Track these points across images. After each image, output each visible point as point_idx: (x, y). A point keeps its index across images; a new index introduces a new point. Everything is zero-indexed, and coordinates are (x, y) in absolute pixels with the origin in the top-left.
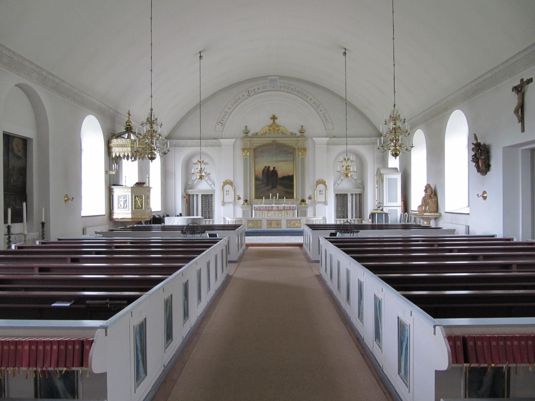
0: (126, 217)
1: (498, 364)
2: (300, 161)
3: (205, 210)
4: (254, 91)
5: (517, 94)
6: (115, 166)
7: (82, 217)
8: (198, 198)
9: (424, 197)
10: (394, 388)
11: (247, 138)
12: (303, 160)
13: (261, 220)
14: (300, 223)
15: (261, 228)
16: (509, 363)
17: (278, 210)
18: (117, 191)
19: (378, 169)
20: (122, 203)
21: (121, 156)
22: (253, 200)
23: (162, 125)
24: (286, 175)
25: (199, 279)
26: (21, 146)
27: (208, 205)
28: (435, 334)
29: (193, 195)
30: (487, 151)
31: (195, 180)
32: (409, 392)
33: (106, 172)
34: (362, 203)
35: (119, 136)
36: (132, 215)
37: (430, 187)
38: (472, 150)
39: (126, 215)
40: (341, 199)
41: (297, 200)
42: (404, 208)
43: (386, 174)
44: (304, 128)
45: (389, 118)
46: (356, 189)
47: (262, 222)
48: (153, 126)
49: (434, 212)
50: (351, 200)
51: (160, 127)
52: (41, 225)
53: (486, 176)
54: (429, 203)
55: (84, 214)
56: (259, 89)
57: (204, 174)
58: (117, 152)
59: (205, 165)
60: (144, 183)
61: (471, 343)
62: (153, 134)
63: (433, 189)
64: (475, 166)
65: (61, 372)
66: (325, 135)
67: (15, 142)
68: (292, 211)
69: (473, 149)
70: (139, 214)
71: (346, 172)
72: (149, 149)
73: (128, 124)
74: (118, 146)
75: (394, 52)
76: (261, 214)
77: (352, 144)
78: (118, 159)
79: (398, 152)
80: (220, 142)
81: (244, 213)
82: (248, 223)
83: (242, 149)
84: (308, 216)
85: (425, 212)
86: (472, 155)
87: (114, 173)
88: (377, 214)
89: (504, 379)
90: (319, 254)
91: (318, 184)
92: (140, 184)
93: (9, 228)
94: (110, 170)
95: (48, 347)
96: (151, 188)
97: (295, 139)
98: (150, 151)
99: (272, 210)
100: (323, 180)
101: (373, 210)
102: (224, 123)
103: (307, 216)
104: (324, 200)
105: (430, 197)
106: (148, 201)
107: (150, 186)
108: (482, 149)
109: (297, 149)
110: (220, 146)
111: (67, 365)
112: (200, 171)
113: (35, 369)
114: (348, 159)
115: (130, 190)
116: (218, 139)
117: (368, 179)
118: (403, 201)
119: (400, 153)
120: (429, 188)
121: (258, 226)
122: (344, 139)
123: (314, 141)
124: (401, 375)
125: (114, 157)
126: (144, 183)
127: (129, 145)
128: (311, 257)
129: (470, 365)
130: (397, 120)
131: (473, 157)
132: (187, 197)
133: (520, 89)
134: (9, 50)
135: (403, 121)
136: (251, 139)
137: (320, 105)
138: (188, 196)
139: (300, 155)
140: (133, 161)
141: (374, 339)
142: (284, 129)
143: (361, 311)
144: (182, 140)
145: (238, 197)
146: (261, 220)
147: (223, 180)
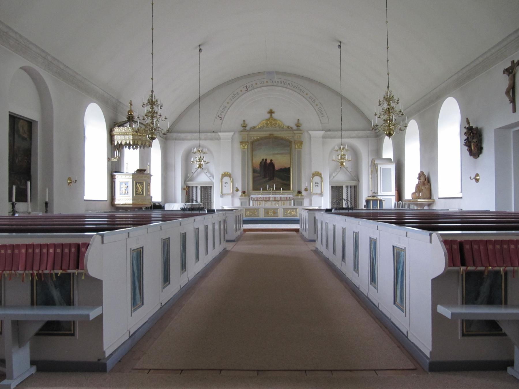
0: (127, 203)
1: (495, 267)
2: (296, 154)
3: (204, 202)
4: (252, 87)
5: (508, 75)
6: (116, 153)
7: (85, 200)
8: (197, 190)
9: (417, 185)
10: (390, 320)
11: (245, 131)
12: (299, 153)
13: (259, 209)
14: (296, 212)
15: (259, 217)
16: (506, 267)
17: (275, 200)
18: (119, 178)
19: (373, 159)
20: (123, 189)
21: (123, 144)
22: (251, 192)
23: (162, 106)
24: (283, 167)
25: (197, 242)
26: (26, 128)
27: (207, 197)
28: (431, 242)
29: (193, 187)
30: (479, 134)
31: (194, 173)
32: (406, 316)
33: (109, 159)
34: (357, 195)
35: (121, 125)
36: (133, 201)
37: (423, 175)
38: (465, 134)
39: (127, 201)
40: (337, 191)
41: (294, 192)
42: (398, 198)
43: (380, 164)
44: (301, 122)
45: (383, 99)
46: (353, 182)
47: (259, 211)
48: (154, 107)
49: (428, 199)
50: (346, 192)
51: (161, 108)
52: (44, 205)
53: (479, 159)
54: (422, 190)
55: (86, 198)
56: (256, 84)
57: (203, 163)
58: (119, 140)
59: (204, 154)
60: (145, 170)
61: (467, 247)
62: (153, 115)
63: (427, 176)
64: (467, 150)
65: (57, 274)
66: (321, 129)
67: (21, 123)
68: (289, 201)
69: (465, 133)
70: (140, 200)
71: (341, 161)
72: (149, 129)
73: (130, 114)
74: (120, 134)
75: (387, 35)
76: (258, 204)
77: (346, 138)
78: (119, 147)
79: (392, 132)
80: (219, 135)
81: (242, 203)
82: (246, 211)
83: (240, 142)
84: (304, 205)
85: (419, 199)
86: (465, 139)
87: (116, 160)
88: (371, 201)
89: (502, 289)
90: (315, 234)
91: (314, 176)
92: (141, 171)
93: (13, 205)
94: (112, 157)
95: (45, 251)
96: (151, 175)
97: (291, 132)
98: (151, 132)
99: (269, 200)
100: (319, 172)
101: (368, 196)
102: (222, 117)
103: (303, 205)
104: (319, 192)
105: (424, 184)
106: (149, 188)
107: (151, 174)
108: (475, 132)
109: (293, 142)
110: (218, 139)
111: (63, 268)
112: (199, 159)
113: (31, 272)
114: (343, 149)
115: (131, 177)
116: (217, 132)
117: (363, 180)
118: (397, 191)
119: (393, 132)
120: (422, 175)
121: (256, 215)
122: (339, 132)
123: (310, 134)
124: (398, 304)
125: (116, 145)
126: (145, 170)
127: (131, 133)
128: (307, 237)
129: (467, 268)
130: (391, 101)
131: (465, 141)
132: (186, 189)
133: (511, 71)
134: (16, 33)
135: (397, 101)
136: (249, 132)
137: (315, 99)
138: (187, 188)
139: (296, 148)
140: (134, 149)
141: (370, 283)
142: (281, 123)
143: (356, 263)
144: (182, 134)
145: (236, 189)
146: (259, 209)
147: (222, 172)
